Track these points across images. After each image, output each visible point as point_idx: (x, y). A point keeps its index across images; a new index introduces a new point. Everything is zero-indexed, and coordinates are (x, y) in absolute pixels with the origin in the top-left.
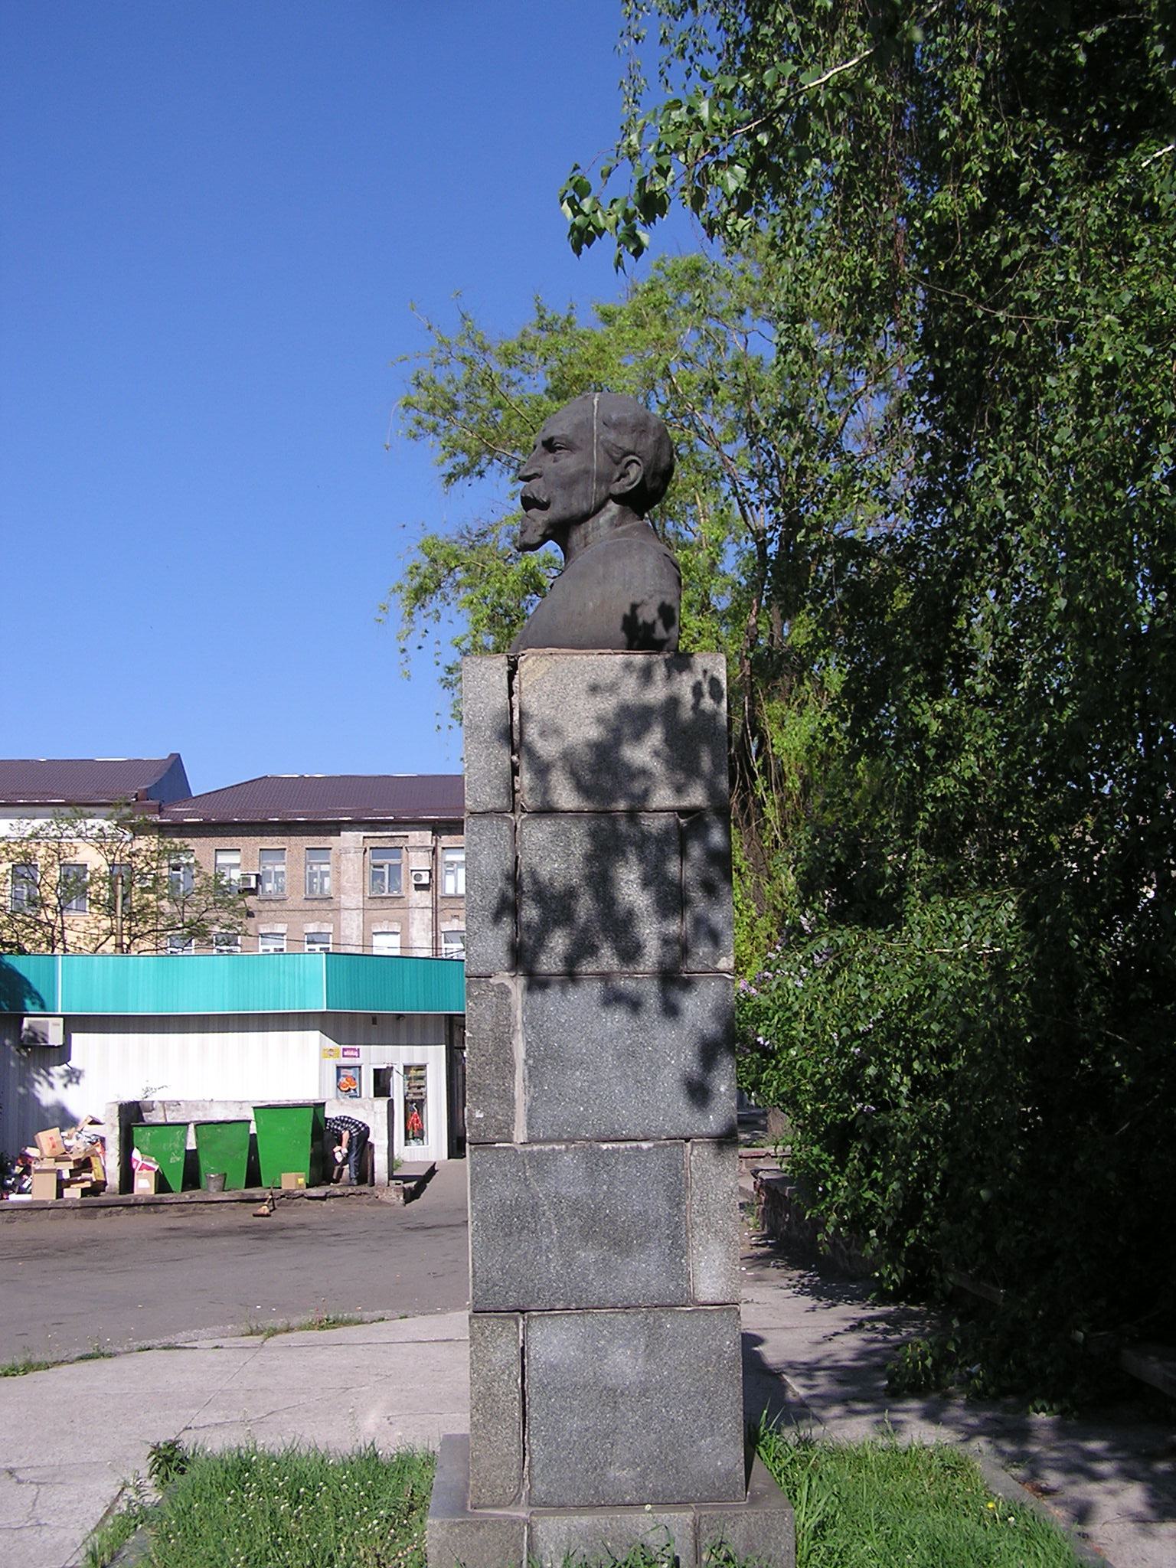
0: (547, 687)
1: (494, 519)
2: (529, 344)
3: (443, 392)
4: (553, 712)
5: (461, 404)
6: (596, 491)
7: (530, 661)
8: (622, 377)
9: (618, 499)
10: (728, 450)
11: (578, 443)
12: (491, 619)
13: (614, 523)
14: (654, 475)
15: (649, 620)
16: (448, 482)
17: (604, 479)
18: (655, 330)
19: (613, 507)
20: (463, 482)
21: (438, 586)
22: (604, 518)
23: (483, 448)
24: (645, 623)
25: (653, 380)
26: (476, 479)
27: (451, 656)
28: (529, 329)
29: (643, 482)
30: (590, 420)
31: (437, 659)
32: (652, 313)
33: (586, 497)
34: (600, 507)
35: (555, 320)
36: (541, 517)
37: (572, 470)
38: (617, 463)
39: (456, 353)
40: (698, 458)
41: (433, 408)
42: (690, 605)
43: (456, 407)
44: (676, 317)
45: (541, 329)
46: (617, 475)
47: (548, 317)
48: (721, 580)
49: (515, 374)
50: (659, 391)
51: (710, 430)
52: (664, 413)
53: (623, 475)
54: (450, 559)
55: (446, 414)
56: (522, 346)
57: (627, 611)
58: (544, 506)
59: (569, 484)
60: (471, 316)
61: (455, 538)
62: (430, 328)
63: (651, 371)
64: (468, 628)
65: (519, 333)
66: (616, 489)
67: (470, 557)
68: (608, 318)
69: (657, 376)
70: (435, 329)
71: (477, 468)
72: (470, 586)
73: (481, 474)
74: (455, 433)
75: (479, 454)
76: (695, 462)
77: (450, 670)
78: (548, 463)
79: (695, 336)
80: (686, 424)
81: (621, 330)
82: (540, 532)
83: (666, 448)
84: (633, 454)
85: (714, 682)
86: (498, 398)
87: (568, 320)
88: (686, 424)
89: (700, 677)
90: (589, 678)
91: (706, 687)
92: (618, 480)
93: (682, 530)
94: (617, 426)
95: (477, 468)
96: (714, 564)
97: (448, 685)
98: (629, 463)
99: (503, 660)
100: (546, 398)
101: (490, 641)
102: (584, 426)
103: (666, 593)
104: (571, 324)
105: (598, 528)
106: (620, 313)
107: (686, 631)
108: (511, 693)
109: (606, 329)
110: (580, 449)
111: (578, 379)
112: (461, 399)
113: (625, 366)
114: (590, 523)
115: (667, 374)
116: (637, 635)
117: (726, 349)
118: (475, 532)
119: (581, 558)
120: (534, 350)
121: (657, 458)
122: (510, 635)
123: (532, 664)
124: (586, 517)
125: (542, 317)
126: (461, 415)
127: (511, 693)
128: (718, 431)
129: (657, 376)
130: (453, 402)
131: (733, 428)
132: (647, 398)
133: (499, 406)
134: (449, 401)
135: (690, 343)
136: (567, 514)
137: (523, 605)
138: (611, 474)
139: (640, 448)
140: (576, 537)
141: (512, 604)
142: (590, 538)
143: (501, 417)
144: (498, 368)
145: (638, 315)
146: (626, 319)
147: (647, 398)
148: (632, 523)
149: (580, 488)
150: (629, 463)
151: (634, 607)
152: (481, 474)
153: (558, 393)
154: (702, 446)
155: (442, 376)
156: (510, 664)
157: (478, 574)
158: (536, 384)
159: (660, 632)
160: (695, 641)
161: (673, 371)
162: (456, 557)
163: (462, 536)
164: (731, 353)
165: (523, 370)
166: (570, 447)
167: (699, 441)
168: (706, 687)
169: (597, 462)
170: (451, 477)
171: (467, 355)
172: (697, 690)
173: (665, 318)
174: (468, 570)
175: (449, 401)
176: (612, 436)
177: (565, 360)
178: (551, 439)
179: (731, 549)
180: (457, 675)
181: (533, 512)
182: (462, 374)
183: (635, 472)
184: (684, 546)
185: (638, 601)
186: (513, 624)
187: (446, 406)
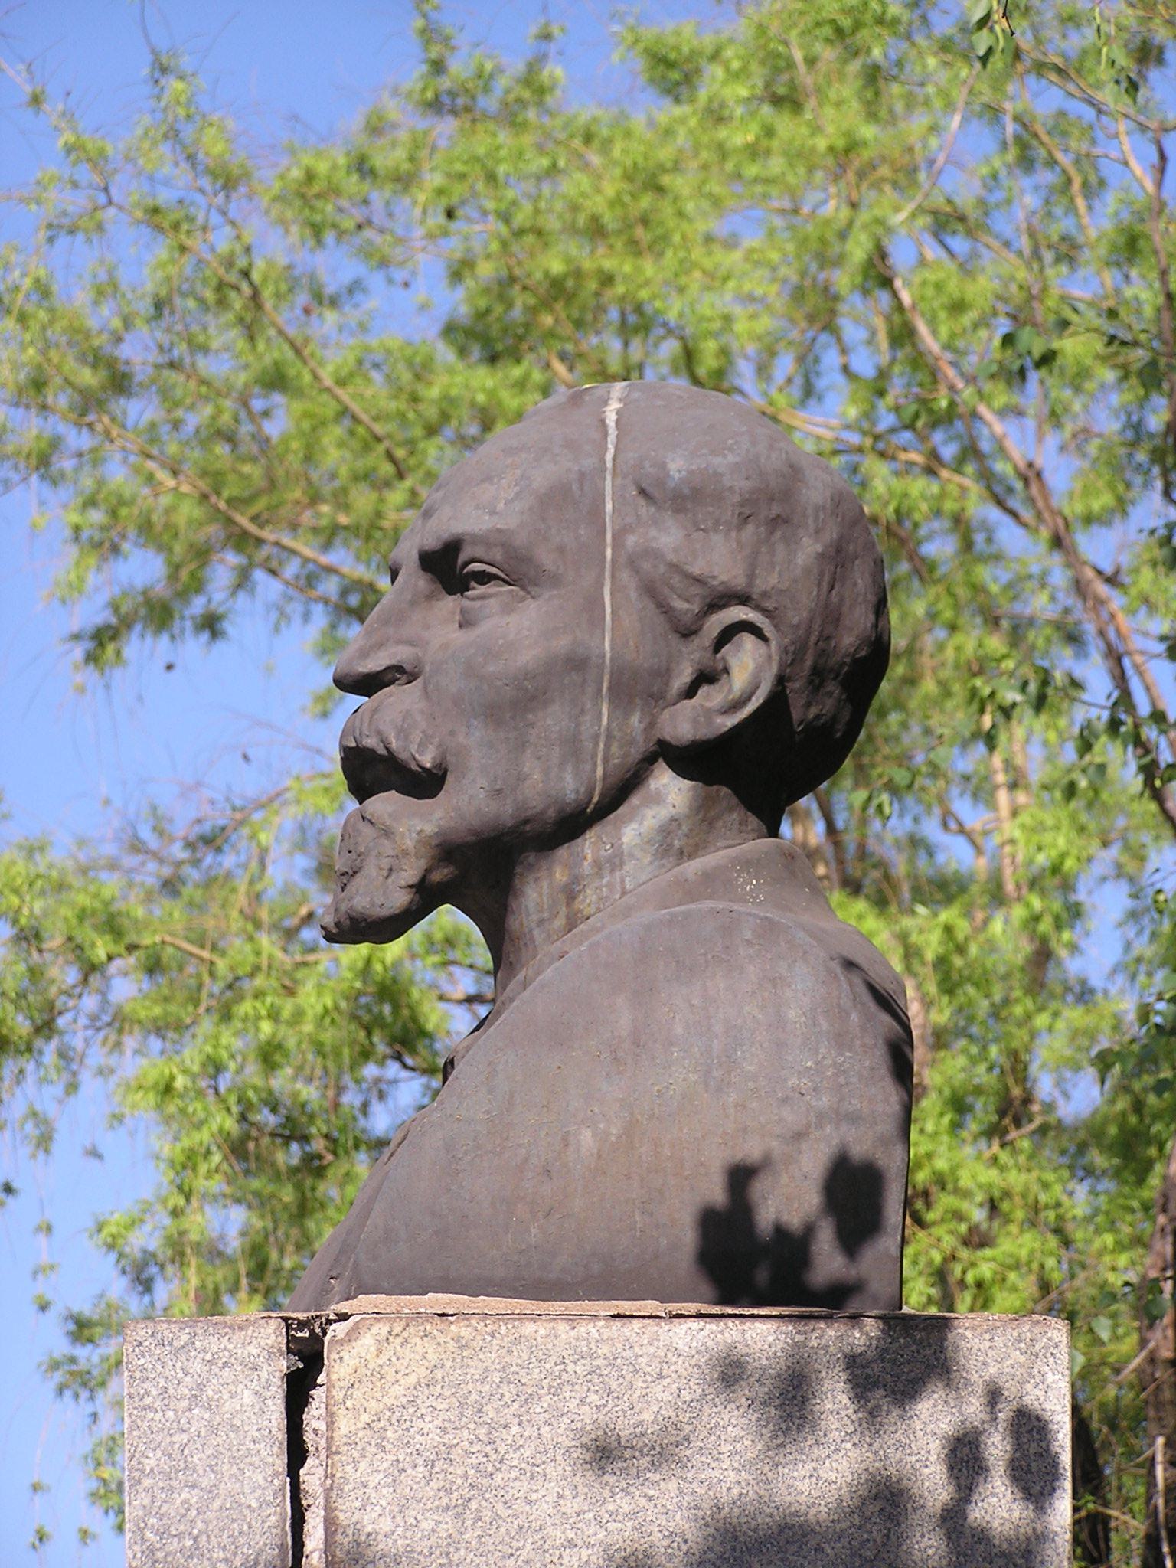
0: (428, 1433)
1: (250, 784)
2: (389, 157)
3: (78, 334)
4: (448, 1524)
5: (141, 373)
6: (608, 732)
7: (367, 1342)
8: (715, 279)
9: (690, 760)
10: (1099, 548)
11: (546, 558)
12: (237, 1149)
13: (672, 846)
14: (818, 676)
15: (794, 1220)
16: (92, 658)
17: (637, 688)
18: (837, 115)
19: (670, 792)
20: (141, 649)
21: (45, 1027)
22: (636, 827)
23: (214, 531)
24: (780, 1231)
25: (831, 296)
26: (193, 647)
27: (92, 1280)
28: (393, 109)
29: (777, 700)
30: (589, 479)
31: (42, 1287)
32: (829, 54)
33: (573, 748)
34: (622, 790)
35: (485, 80)
36: (412, 824)
37: (527, 657)
38: (687, 633)
39: (129, 190)
40: (984, 573)
41: (38, 384)
42: (959, 1105)
43: (120, 382)
44: (914, 70)
45: (435, 106)
46: (684, 676)
47: (459, 68)
48: (1074, 1015)
49: (335, 266)
50: (852, 332)
51: (1031, 475)
52: (869, 415)
53: (706, 677)
54: (87, 934)
55: (87, 404)
56: (362, 167)
57: (716, 1193)
58: (425, 784)
59: (515, 704)
60: (186, 62)
61: (109, 849)
62: (36, 100)
63: (825, 260)
64: (152, 1181)
65: (355, 123)
66: (684, 723)
67: (163, 923)
68: (673, 74)
69: (842, 280)
70: (54, 107)
71: (198, 605)
72: (159, 1028)
73: (211, 625)
74: (118, 475)
75: (202, 554)
76: (978, 589)
77: (81, 1329)
78: (439, 630)
79: (983, 138)
80: (949, 452)
81: (716, 115)
82: (410, 873)
83: (860, 580)
84: (744, 599)
85: (1028, 1427)
86: (272, 351)
87: (528, 78)
88: (949, 452)
89: (974, 1408)
90: (585, 1411)
91: (997, 1447)
92: (690, 692)
93: (931, 828)
94: (685, 500)
95: (198, 605)
96: (1043, 956)
97: (81, 1382)
98: (727, 635)
99: (272, 1334)
100: (445, 354)
101: (229, 1223)
102: (567, 500)
103: (853, 1118)
104: (541, 91)
105: (616, 861)
106: (715, 56)
107: (944, 1201)
108: (297, 1453)
109: (667, 112)
110: (555, 581)
111: (558, 290)
112: (138, 352)
113: (731, 243)
114: (590, 846)
115: (879, 275)
116: (739, 1260)
117: (1093, 190)
118: (181, 827)
119: (553, 973)
120: (405, 181)
121: (831, 616)
122: (303, 1209)
123: (378, 1354)
124: (574, 823)
125: (438, 67)
126: (140, 411)
127: (297, 1453)
128: (1062, 475)
129: (842, 280)
130: (111, 364)
131: (1117, 467)
132: (808, 360)
133: (276, 381)
134: (97, 359)
135: (962, 155)
136: (505, 812)
137: (351, 1099)
138: (664, 674)
139: (768, 581)
140: (536, 894)
141: (309, 1093)
142: (588, 900)
143: (282, 421)
144: (276, 247)
145: (778, 63)
146: (735, 76)
147: (808, 360)
148: (738, 845)
149: (553, 719)
150: (727, 635)
151: (741, 1177)
152: (211, 625)
153: (487, 339)
154: (1010, 536)
155: (74, 275)
156: (293, 1347)
157: (189, 987)
158: (410, 307)
159: (828, 1262)
160: (977, 1240)
161: (901, 257)
162: (112, 925)
163: (137, 846)
164: (1111, 201)
165: (366, 253)
166: (516, 573)
167: (994, 514)
168: (997, 1447)
169: (618, 630)
170: (102, 641)
171: (164, 197)
172: (965, 1458)
173: (873, 76)
174: (153, 967)
175: (97, 359)
176: (668, 537)
177: (520, 218)
178: (453, 547)
179: (1107, 902)
180: (109, 1347)
181: (386, 803)
182: (146, 265)
183: (749, 667)
184: (944, 889)
185: (751, 1150)
186: (313, 1167)
187: (87, 377)
